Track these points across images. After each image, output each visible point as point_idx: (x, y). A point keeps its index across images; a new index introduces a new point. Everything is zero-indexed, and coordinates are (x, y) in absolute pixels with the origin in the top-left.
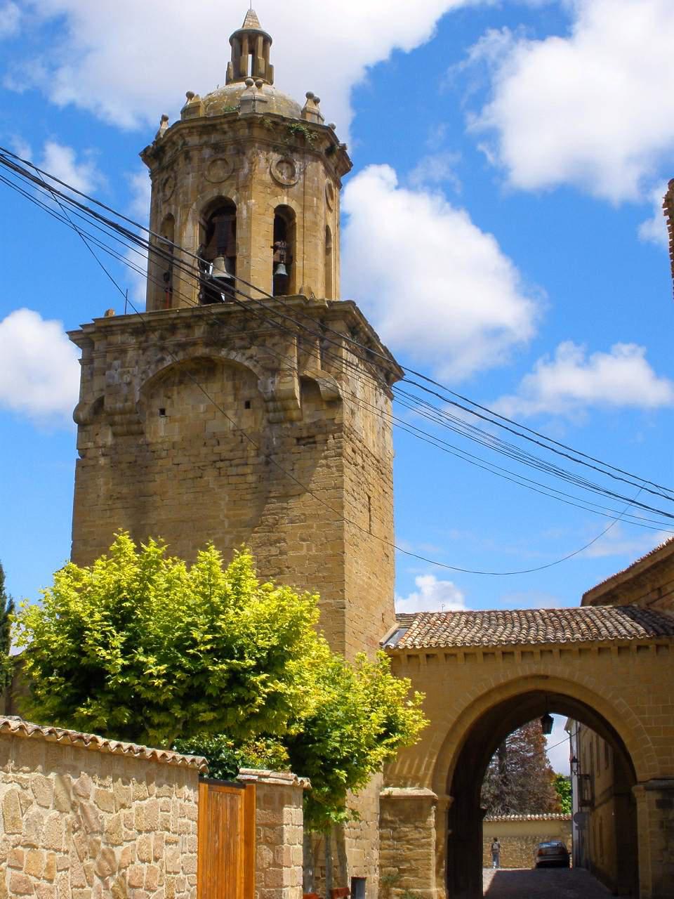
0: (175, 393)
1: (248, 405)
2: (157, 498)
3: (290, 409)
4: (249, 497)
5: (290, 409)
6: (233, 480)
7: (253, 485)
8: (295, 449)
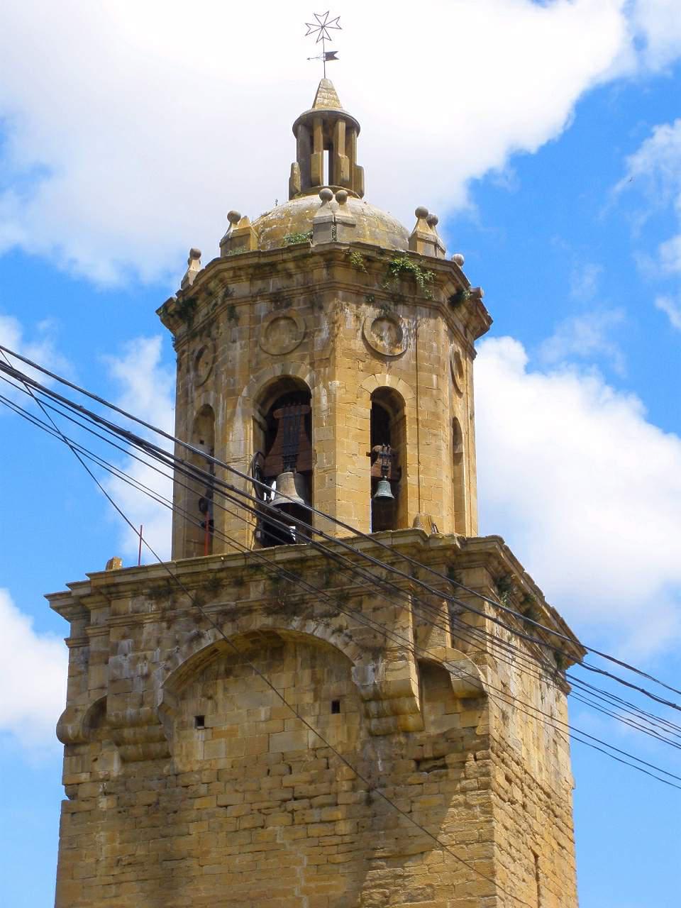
2: (193, 863)
6: (314, 830)
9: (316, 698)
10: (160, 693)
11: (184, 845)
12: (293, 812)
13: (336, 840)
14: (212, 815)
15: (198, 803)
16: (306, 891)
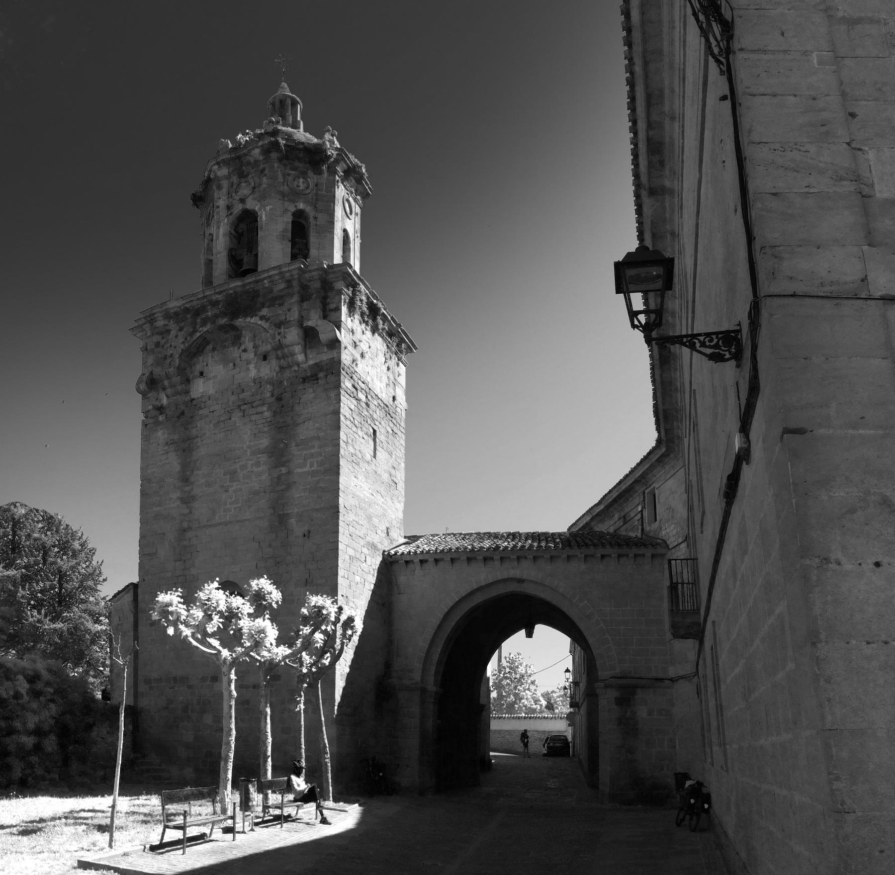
0: (210, 358)
1: (265, 358)
2: (199, 439)
3: (295, 354)
4: (266, 429)
5: (295, 354)
6: (253, 418)
7: (269, 420)
8: (301, 387)
9: (255, 354)
10: (177, 361)
11: (194, 432)
12: (244, 411)
13: (264, 421)
14: (207, 416)
15: (201, 412)
16: (249, 447)
